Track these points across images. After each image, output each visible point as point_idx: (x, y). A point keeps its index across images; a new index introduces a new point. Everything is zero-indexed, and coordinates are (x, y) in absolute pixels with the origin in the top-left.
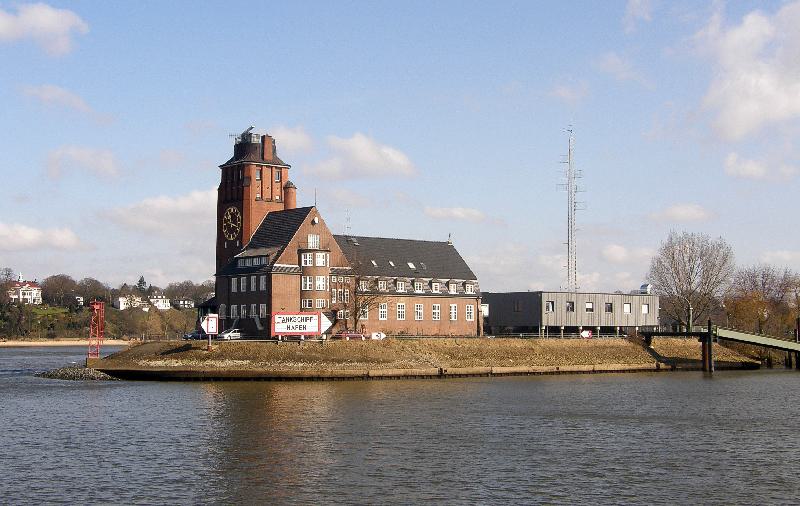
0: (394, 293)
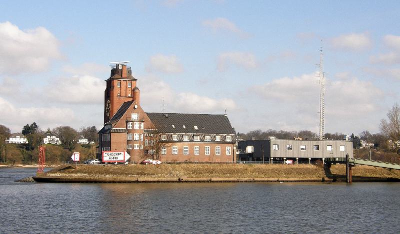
0: (181, 141)
